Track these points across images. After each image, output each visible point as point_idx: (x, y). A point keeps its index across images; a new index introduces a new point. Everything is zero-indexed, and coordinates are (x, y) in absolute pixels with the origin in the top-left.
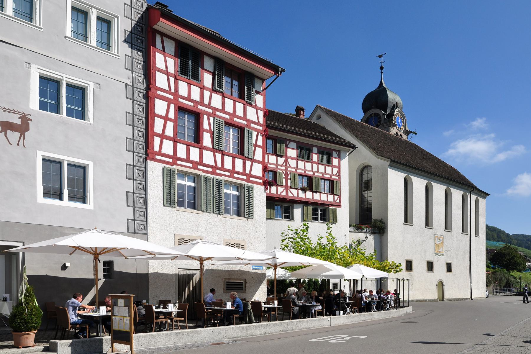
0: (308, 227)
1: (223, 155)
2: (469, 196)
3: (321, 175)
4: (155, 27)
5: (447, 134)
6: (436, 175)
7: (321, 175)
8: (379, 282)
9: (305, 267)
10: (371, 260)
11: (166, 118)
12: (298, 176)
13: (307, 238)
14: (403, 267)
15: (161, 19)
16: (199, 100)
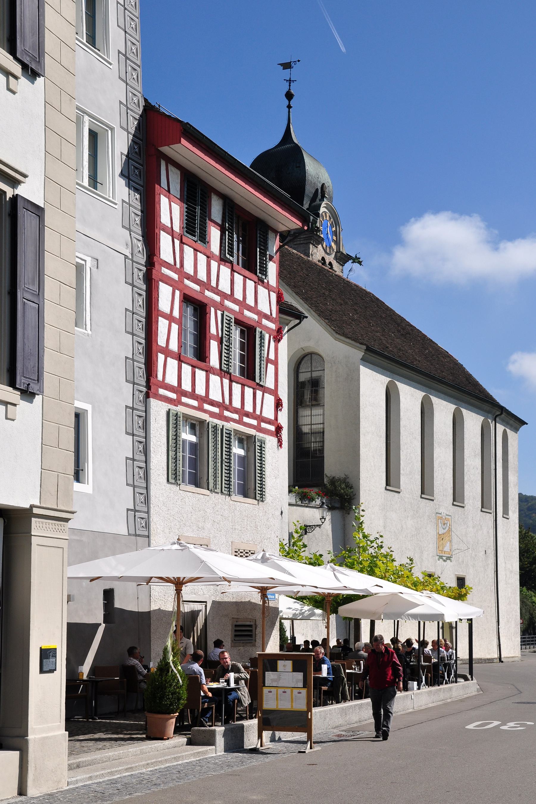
1: (231, 381)
2: (492, 426)
6: (440, 381)
15: (183, 141)
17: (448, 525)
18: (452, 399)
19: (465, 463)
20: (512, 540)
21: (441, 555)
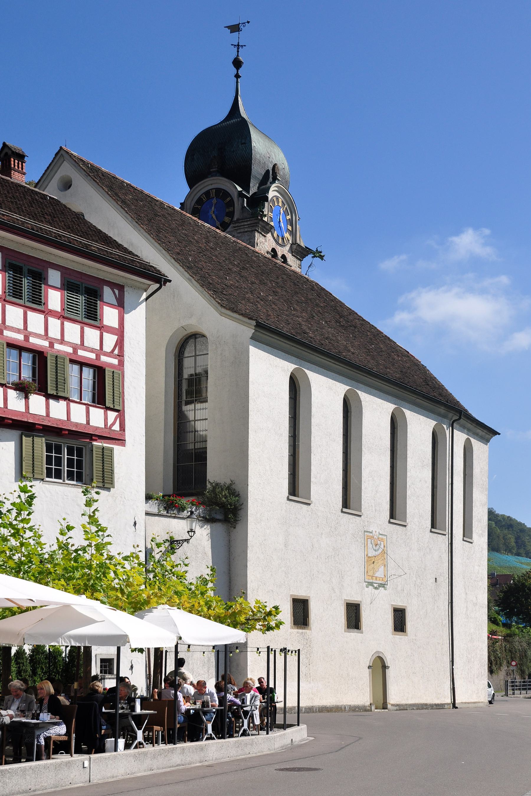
0: (32, 497)
2: (448, 433)
3: (70, 350)
5: (390, 265)
6: (369, 373)
7: (70, 350)
8: (222, 656)
9: (22, 611)
10: (202, 594)
12: (6, 350)
13: (31, 529)
14: (286, 614)
17: (382, 546)
18: (390, 397)
19: (409, 474)
20: (477, 567)
21: (371, 581)
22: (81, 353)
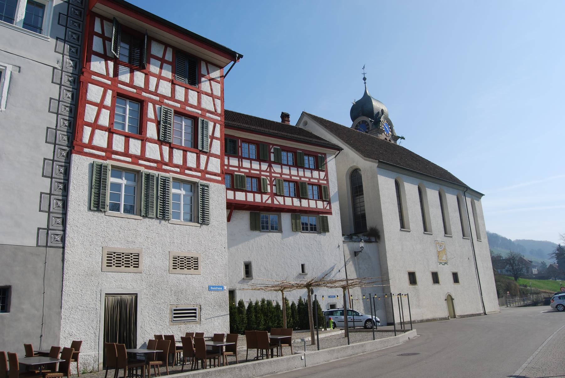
1: (171, 148)
4: (94, 10)
7: (307, 180)
11: (101, 106)
16: (143, 86)
22: (312, 180)
